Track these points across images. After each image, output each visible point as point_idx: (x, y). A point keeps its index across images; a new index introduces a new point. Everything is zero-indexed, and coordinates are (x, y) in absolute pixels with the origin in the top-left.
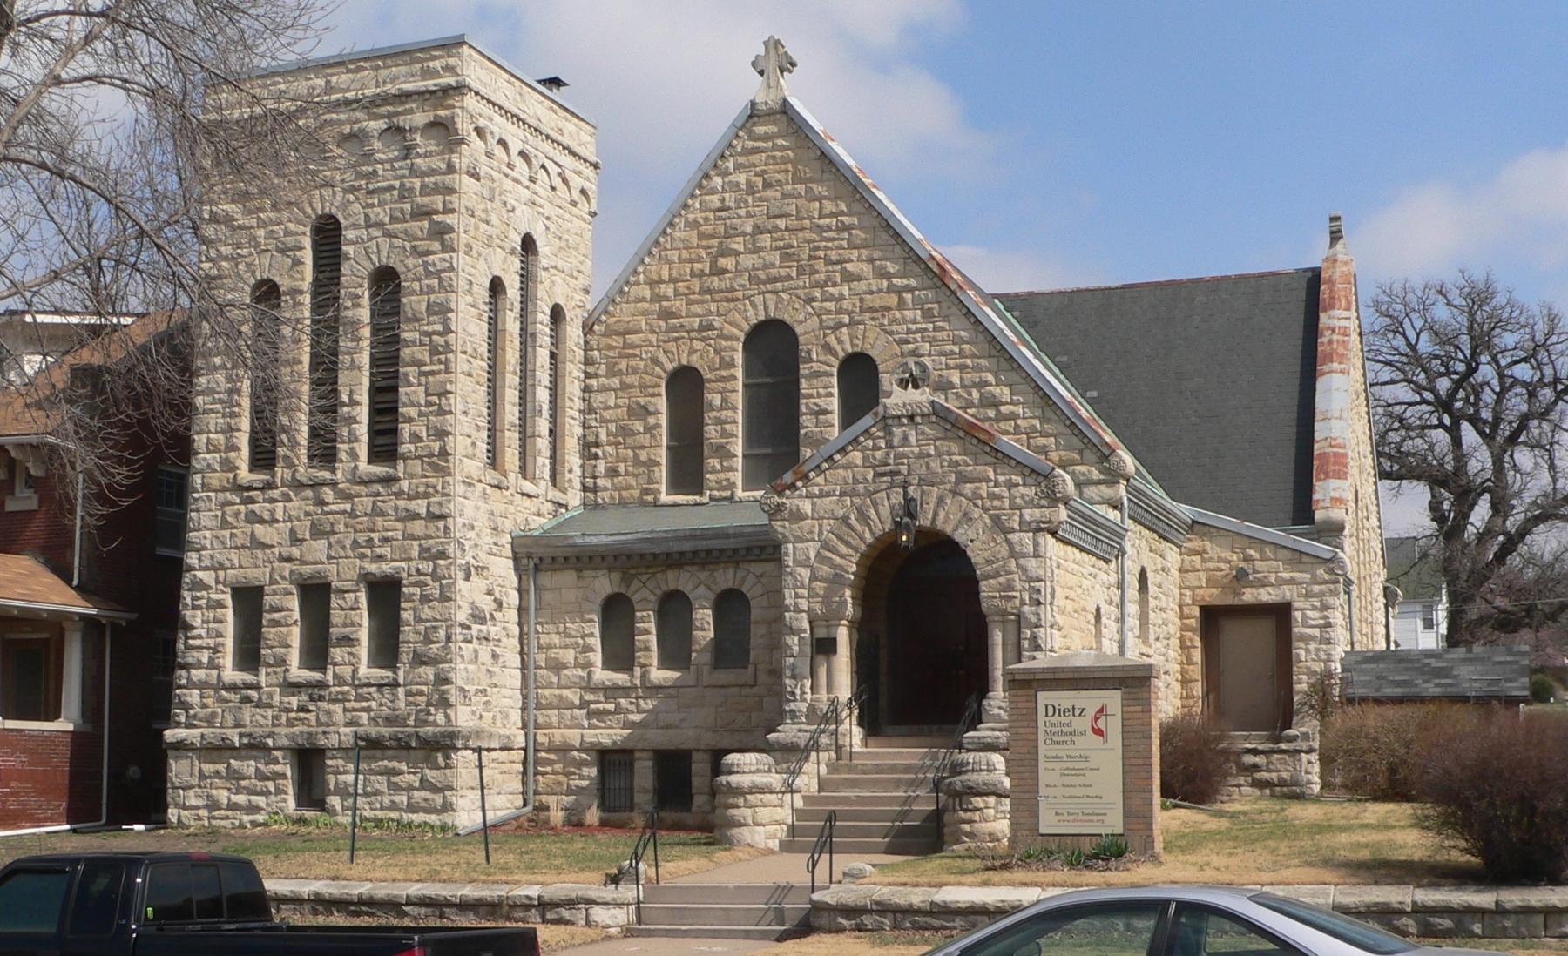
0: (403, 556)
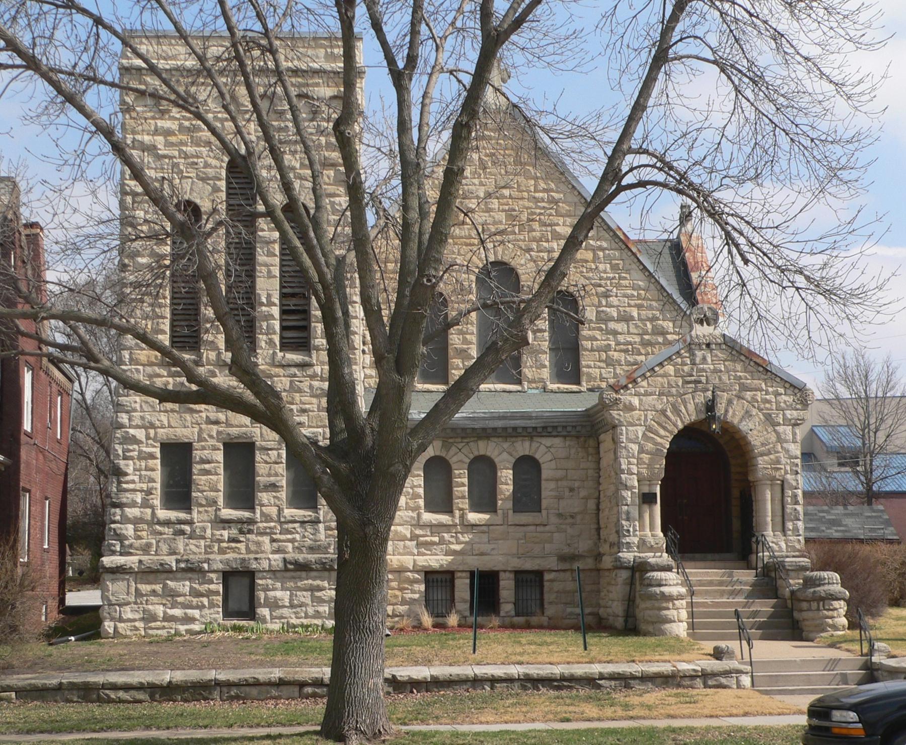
0: (319, 424)
